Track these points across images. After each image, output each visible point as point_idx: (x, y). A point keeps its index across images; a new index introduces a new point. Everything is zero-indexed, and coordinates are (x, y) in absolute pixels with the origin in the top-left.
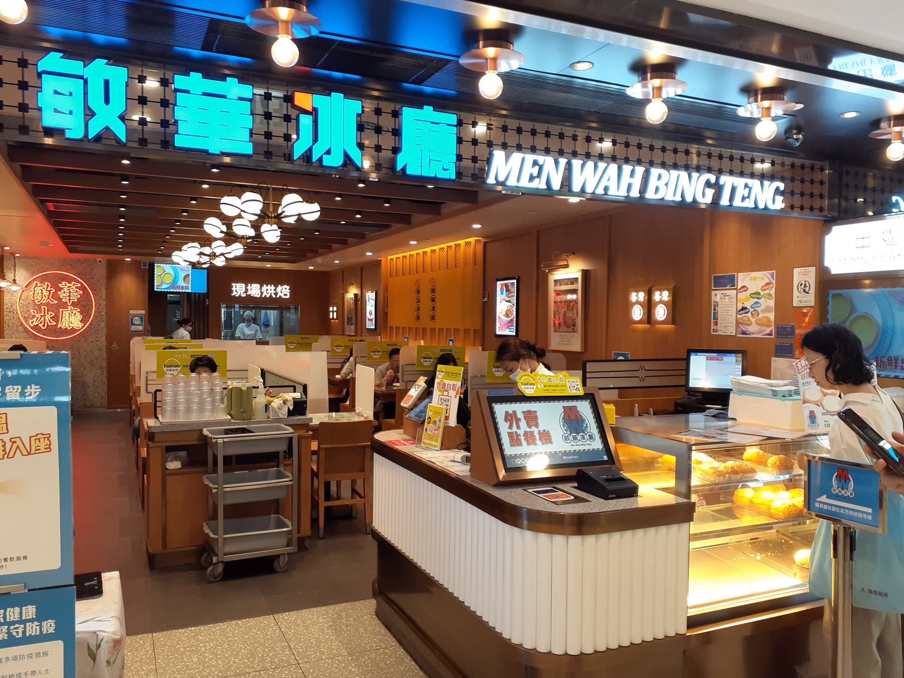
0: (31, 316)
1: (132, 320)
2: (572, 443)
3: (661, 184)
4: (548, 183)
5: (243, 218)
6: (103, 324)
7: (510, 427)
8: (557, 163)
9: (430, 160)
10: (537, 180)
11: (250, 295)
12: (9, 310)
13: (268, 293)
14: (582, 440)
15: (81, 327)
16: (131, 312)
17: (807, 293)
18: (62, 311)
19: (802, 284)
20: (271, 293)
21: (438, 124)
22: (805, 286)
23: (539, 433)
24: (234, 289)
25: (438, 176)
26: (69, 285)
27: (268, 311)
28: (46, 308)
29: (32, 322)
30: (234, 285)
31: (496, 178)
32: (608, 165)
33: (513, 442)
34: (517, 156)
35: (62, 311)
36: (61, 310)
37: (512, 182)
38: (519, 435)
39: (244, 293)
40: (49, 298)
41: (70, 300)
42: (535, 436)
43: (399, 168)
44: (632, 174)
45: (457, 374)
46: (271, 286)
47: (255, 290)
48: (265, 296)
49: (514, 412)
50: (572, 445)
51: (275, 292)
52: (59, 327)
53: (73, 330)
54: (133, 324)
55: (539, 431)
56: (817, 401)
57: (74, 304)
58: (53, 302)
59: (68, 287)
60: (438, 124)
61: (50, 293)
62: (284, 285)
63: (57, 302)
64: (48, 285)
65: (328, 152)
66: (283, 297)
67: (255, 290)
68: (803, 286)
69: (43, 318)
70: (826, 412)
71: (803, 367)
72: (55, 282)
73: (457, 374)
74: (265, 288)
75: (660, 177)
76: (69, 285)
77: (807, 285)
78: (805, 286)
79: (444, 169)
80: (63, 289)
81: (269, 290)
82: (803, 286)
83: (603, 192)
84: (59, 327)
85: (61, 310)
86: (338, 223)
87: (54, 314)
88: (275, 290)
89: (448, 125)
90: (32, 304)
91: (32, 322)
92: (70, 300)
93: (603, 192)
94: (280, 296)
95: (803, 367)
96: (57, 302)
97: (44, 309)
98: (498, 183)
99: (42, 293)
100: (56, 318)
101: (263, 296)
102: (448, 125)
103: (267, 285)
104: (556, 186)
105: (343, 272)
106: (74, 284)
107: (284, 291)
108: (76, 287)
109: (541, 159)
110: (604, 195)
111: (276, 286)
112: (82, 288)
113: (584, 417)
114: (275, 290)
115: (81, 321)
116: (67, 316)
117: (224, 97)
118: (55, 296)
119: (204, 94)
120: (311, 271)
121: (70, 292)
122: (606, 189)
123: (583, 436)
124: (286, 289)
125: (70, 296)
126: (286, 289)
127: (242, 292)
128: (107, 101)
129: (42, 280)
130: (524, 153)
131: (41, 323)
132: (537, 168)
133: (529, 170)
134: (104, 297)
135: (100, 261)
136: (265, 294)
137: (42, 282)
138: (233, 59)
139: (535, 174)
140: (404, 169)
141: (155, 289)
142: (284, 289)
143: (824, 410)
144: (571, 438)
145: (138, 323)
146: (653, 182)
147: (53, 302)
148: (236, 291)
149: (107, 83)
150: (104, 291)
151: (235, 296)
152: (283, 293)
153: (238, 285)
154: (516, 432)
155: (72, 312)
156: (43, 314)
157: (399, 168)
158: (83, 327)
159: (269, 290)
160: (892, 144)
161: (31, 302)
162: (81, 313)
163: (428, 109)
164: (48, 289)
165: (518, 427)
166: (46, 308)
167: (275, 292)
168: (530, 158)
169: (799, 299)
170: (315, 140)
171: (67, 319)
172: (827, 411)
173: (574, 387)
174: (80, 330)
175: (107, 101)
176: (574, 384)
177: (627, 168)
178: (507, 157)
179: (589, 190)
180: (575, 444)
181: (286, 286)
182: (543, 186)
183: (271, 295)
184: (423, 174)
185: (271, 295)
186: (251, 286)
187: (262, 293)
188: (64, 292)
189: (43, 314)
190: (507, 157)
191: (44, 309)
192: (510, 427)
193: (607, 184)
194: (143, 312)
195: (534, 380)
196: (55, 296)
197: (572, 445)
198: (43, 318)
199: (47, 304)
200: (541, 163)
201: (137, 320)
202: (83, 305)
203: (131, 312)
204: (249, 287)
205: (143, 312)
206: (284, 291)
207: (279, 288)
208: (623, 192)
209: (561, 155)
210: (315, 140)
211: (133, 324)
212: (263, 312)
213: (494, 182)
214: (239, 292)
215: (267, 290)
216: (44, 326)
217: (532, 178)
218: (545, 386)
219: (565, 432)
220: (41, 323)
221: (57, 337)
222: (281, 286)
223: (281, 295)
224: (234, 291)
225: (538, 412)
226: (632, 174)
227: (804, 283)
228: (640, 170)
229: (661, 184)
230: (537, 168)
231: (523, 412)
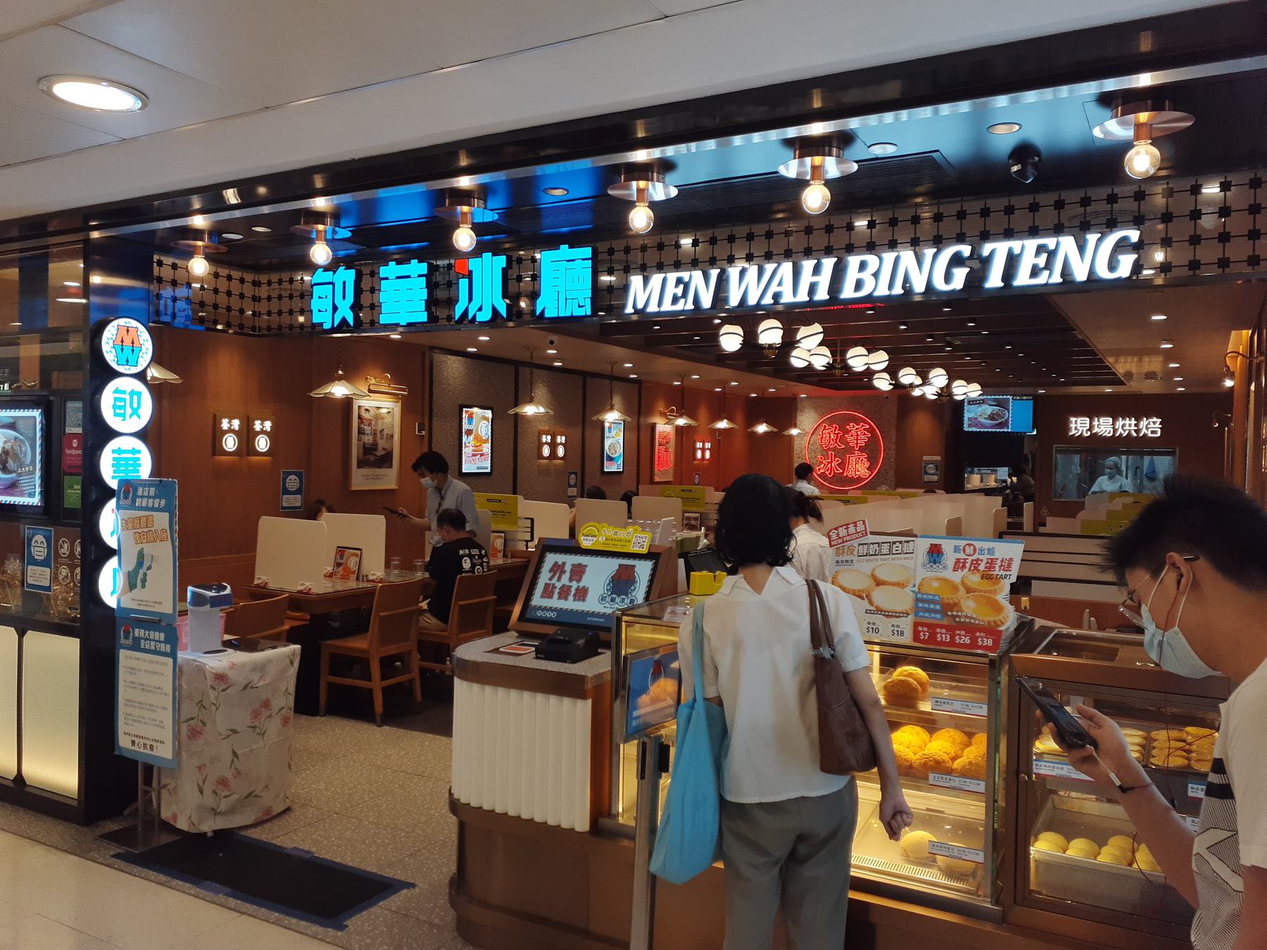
1: (925, 467)
2: (607, 605)
3: (867, 276)
4: (696, 301)
5: (818, 346)
6: (892, 473)
7: (551, 579)
8: (706, 277)
9: (566, 299)
10: (682, 301)
11: (1096, 433)
12: (798, 456)
13: (1124, 430)
14: (620, 604)
15: (868, 475)
16: (925, 458)
18: (849, 457)
20: (1130, 430)
21: (573, 260)
24: (1073, 425)
25: (574, 314)
26: (857, 427)
28: (833, 453)
29: (819, 470)
30: (1073, 419)
31: (634, 306)
32: (779, 264)
33: (545, 593)
34: (657, 279)
35: (849, 457)
36: (848, 456)
37: (653, 308)
38: (556, 588)
39: (1087, 430)
40: (836, 442)
41: (857, 444)
42: (571, 591)
43: (538, 312)
44: (817, 270)
45: (503, 512)
46: (1130, 420)
47: (1104, 426)
48: (1121, 434)
49: (564, 564)
51: (1136, 428)
52: (845, 475)
53: (860, 479)
54: (926, 473)
55: (579, 586)
56: (859, 591)
57: (861, 449)
58: (840, 446)
59: (857, 429)
60: (573, 260)
61: (837, 436)
62: (1152, 418)
63: (844, 447)
64: (836, 428)
65: (480, 309)
66: (1150, 435)
67: (1104, 426)
69: (830, 465)
70: (873, 608)
71: (840, 538)
72: (842, 424)
73: (503, 512)
74: (1120, 422)
75: (863, 266)
76: (857, 427)
79: (579, 306)
80: (850, 431)
81: (1126, 426)
83: (772, 302)
84: (845, 475)
85: (848, 456)
86: (980, 334)
87: (840, 461)
89: (583, 259)
90: (820, 449)
91: (819, 470)
92: (857, 444)
93: (772, 302)
94: (1145, 435)
95: (840, 538)
96: (844, 447)
97: (832, 454)
98: (637, 311)
99: (830, 437)
100: (842, 465)
101: (1117, 435)
102: (583, 259)
103: (1123, 419)
104: (706, 302)
106: (863, 426)
107: (1151, 427)
108: (864, 429)
109: (685, 275)
110: (773, 304)
111: (1138, 419)
112: (871, 430)
113: (637, 579)
114: (1136, 425)
115: (868, 469)
117: (408, 277)
118: (842, 439)
119: (398, 278)
120: (1181, 393)
121: (858, 435)
122: (776, 296)
123: (623, 599)
124: (1154, 423)
125: (857, 440)
126: (1154, 423)
127: (1085, 429)
128: (344, 298)
129: (831, 421)
130: (665, 273)
131: (827, 470)
132: (682, 286)
133: (671, 290)
134: (894, 439)
135: (887, 398)
136: (1120, 430)
137: (830, 425)
138: (392, 247)
139: (680, 294)
140: (543, 312)
141: (966, 428)
142: (1151, 423)
143: (872, 605)
144: (608, 599)
145: (933, 472)
146: (852, 275)
147: (840, 446)
148: (1076, 428)
149: (344, 283)
150: (894, 433)
151: (1074, 435)
152: (1150, 430)
153: (1079, 420)
155: (859, 459)
156: (830, 461)
157: (538, 312)
158: (870, 476)
159: (1126, 426)
161: (819, 446)
162: (869, 459)
163: (564, 247)
164: (836, 432)
166: (833, 453)
167: (1136, 428)
168: (672, 277)
170: (470, 299)
171: (854, 466)
172: (876, 607)
173: (639, 543)
174: (867, 479)
175: (344, 298)
176: (640, 540)
177: (808, 265)
178: (646, 281)
179: (752, 301)
180: (609, 606)
181: (1155, 419)
182: (690, 306)
183: (1129, 434)
184: (560, 315)
185: (1129, 434)
186: (1098, 421)
187: (1115, 431)
188: (852, 436)
189: (830, 461)
190: (646, 281)
191: (832, 454)
192: (551, 579)
193: (779, 289)
194: (939, 458)
195: (598, 531)
196: (842, 439)
197: (605, 607)
198: (830, 465)
199: (834, 449)
200: (686, 279)
201: (931, 469)
202: (870, 450)
203: (925, 458)
204: (1096, 423)
205: (939, 458)
206: (1151, 427)
207: (1144, 423)
208: (803, 296)
209: (677, 268)
210: (470, 299)
211: (926, 473)
212: (1147, 459)
213: (633, 311)
214: (1081, 429)
215: (1124, 426)
216: (830, 474)
217: (675, 300)
218: (606, 539)
219: (606, 592)
220: (827, 470)
221: (843, 486)
222: (1147, 419)
223: (1147, 432)
224: (1073, 429)
225: (557, 561)
226: (817, 270)
228: (829, 263)
229: (867, 276)
230: (682, 286)
231: (586, 566)
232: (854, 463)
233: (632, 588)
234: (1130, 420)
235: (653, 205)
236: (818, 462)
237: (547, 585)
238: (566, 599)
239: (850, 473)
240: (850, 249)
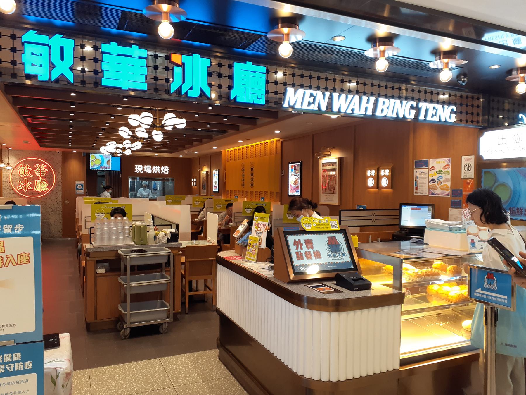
1: (77, 186)
2: (333, 258)
3: (385, 107)
4: (319, 106)
5: (141, 127)
6: (60, 189)
7: (297, 249)
8: (324, 95)
9: (250, 93)
10: (312, 105)
11: (145, 172)
12: (5, 181)
13: (156, 171)
14: (339, 256)
15: (47, 190)
16: (76, 182)
17: (470, 171)
18: (36, 181)
19: (466, 165)
20: (158, 171)
21: (255, 72)
22: (469, 166)
23: (314, 252)
24: (136, 168)
25: (255, 103)
26: (40, 166)
28: (27, 179)
29: (19, 188)
30: (136, 166)
31: (289, 104)
32: (354, 96)
33: (298, 257)
34: (301, 91)
35: (36, 181)
36: (35, 181)
37: (298, 106)
38: (302, 254)
39: (142, 171)
40: (28, 174)
41: (40, 175)
42: (311, 254)
43: (232, 98)
44: (368, 101)
46: (158, 167)
47: (148, 169)
48: (154, 172)
49: (299, 240)
51: (160, 170)
52: (34, 190)
53: (43, 192)
54: (77, 189)
55: (314, 251)
56: (475, 234)
57: (43, 177)
58: (31, 176)
59: (40, 167)
60: (255, 72)
61: (29, 171)
62: (165, 166)
63: (33, 176)
64: (28, 166)
65: (191, 89)
66: (165, 173)
67: (148, 169)
68: (467, 167)
69: (25, 186)
70: (480, 240)
71: (467, 214)
74: (154, 168)
75: (384, 103)
76: (40, 166)
77: (470, 166)
78: (469, 166)
79: (258, 99)
80: (36, 168)
81: (156, 169)
82: (467, 167)
83: (351, 112)
84: (34, 190)
85: (35, 181)
86: (197, 130)
87: (31, 183)
88: (160, 169)
89: (261, 73)
90: (18, 177)
91: (19, 188)
92: (40, 175)
94: (163, 173)
95: (467, 214)
96: (33, 176)
97: (26, 180)
98: (290, 107)
99: (24, 171)
100: (32, 185)
101: (153, 172)
102: (261, 73)
103: (155, 166)
104: (324, 108)
105: (199, 158)
106: (43, 166)
107: (165, 170)
108: (44, 167)
109: (315, 92)
110: (351, 113)
111: (161, 167)
112: (48, 168)
113: (340, 243)
114: (160, 169)
115: (47, 187)
117: (130, 56)
118: (32, 173)
119: (119, 55)
120: (181, 158)
121: (41, 170)
122: (353, 110)
123: (339, 254)
124: (166, 168)
126: (166, 168)
127: (141, 170)
128: (62, 59)
130: (305, 89)
131: (24, 188)
132: (312, 98)
133: (308, 99)
134: (61, 173)
135: (58, 152)
136: (154, 171)
137: (24, 165)
138: (135, 34)
139: (311, 101)
140: (235, 98)
141: (90, 169)
142: (165, 168)
143: (480, 239)
144: (332, 255)
145: (81, 188)
146: (380, 106)
147: (31, 176)
148: (137, 170)
149: (62, 48)
150: (60, 169)
152: (165, 171)
153: (139, 166)
154: (300, 252)
155: (42, 182)
156: (25, 183)
157: (232, 98)
158: (48, 191)
159: (156, 169)
161: (18, 176)
162: (47, 182)
163: (249, 63)
164: (28, 168)
166: (27, 179)
167: (160, 170)
168: (308, 92)
169: (465, 174)
170: (184, 81)
172: (481, 239)
173: (334, 225)
174: (46, 192)
175: (62, 59)
176: (334, 224)
177: (365, 98)
178: (295, 92)
179: (343, 110)
180: (335, 259)
181: (166, 167)
182: (316, 108)
183: (158, 172)
184: (246, 102)
185: (158, 172)
186: (146, 167)
187: (152, 171)
188: (37, 170)
189: (25, 183)
190: (295, 92)
191: (26, 180)
192: (297, 249)
193: (353, 107)
194: (83, 182)
195: (311, 221)
196: (32, 173)
197: (333, 259)
198: (25, 186)
199: (27, 177)
200: (315, 95)
201: (80, 187)
202: (48, 178)
203: (76, 182)
204: (145, 167)
205: (83, 182)
206: (165, 170)
207: (162, 168)
208: (362, 112)
209: (326, 91)
210: (184, 81)
211: (77, 189)
212: (153, 182)
213: (288, 106)
214: (139, 170)
215: (155, 169)
216: (25, 190)
217: (309, 104)
218: (317, 225)
219: (329, 252)
220: (24, 188)
221: (33, 196)
222: (164, 167)
223: (164, 172)
224: (136, 170)
225: (313, 240)
226: (368, 101)
227: (468, 165)
228: (372, 99)
230: (312, 98)
231: (304, 240)
232: (39, 184)
233: (340, 248)
234: (158, 167)
235: (388, 59)
236: (18, 184)
237: (297, 253)
238: (303, 259)
239: (37, 189)
240: (379, 95)
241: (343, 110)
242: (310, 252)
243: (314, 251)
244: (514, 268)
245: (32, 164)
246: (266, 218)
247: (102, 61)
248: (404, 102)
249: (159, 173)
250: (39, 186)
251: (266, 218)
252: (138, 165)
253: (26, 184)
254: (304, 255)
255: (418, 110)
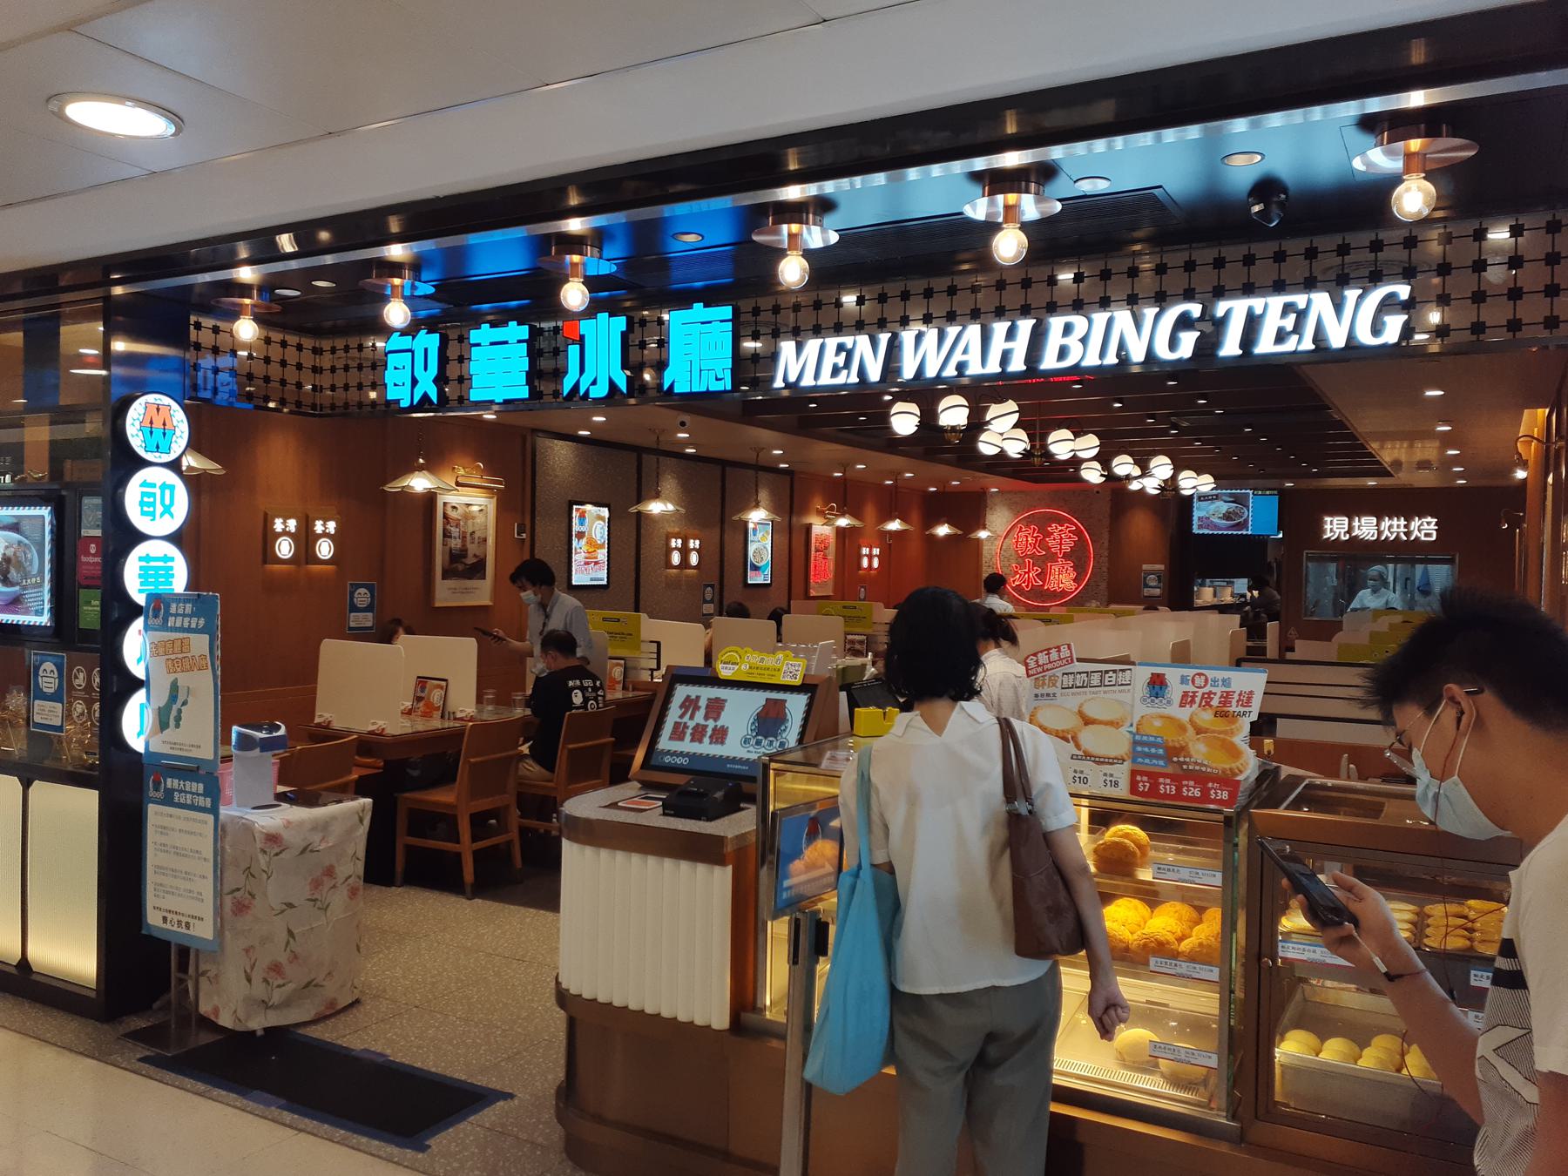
0: (1013, 572)
1: (1145, 578)
2: (751, 749)
3: (1073, 341)
4: (862, 372)
5: (1013, 428)
6: (1103, 585)
7: (682, 716)
8: (874, 343)
9: (701, 370)
10: (845, 372)
11: (1356, 537)
12: (987, 564)
13: (1391, 533)
14: (767, 747)
15: (1074, 588)
16: (1145, 567)
18: (1051, 566)
20: (1398, 533)
21: (710, 322)
23: (714, 730)
24: (1328, 527)
25: (711, 389)
26: (1060, 528)
27: (1430, 567)
28: (1031, 561)
29: (1014, 581)
30: (1328, 519)
31: (785, 379)
32: (964, 327)
33: (675, 734)
34: (812, 345)
35: (1051, 566)
36: (1049, 564)
37: (808, 381)
38: (687, 728)
39: (1345, 533)
40: (1035, 548)
41: (1061, 549)
42: (706, 732)
43: (666, 387)
44: (1011, 334)
46: (1398, 520)
47: (1366, 528)
48: (1387, 538)
49: (698, 698)
50: (748, 751)
51: (1406, 530)
52: (1046, 588)
53: (1064, 593)
54: (1146, 586)
55: (716, 726)
56: (1063, 731)
57: (1066, 556)
58: (1039, 552)
59: (1060, 531)
60: (710, 322)
61: (1036, 540)
62: (1425, 517)
63: (1044, 553)
64: (1034, 529)
65: (594, 383)
66: (1423, 538)
67: (1366, 528)
69: (1027, 576)
70: (1081, 753)
71: (1039, 666)
74: (1386, 523)
75: (1068, 329)
76: (1060, 528)
79: (717, 379)
80: (1052, 534)
81: (1393, 527)
83: (956, 373)
84: (1046, 588)
85: (1049, 564)
86: (1212, 413)
87: (1040, 570)
88: (1405, 526)
89: (722, 321)
90: (1014, 556)
91: (1014, 581)
92: (1061, 549)
94: (1417, 538)
95: (1039, 666)
96: (1044, 553)
97: (1029, 562)
98: (788, 386)
99: (1027, 541)
100: (1042, 576)
101: (1383, 538)
102: (722, 321)
103: (1390, 518)
104: (874, 374)
106: (1068, 527)
107: (1425, 528)
108: (1070, 531)
109: (848, 341)
110: (956, 377)
111: (1408, 519)
112: (1078, 532)
113: (789, 717)
114: (1405, 526)
115: (1074, 581)
116: (1057, 573)
117: (506, 343)
118: (1042, 544)
119: (492, 344)
120: (1462, 487)
121: (1061, 539)
122: (961, 367)
123: (771, 741)
124: (1428, 523)
126: (1428, 523)
127: (1343, 531)
128: (426, 369)
130: (824, 338)
131: (1024, 582)
132: (844, 354)
133: (831, 358)
134: (1106, 544)
135: (1098, 492)
136: (1386, 533)
137: (1027, 526)
138: (486, 306)
139: (841, 364)
140: (672, 386)
141: (1196, 530)
142: (1425, 524)
144: (753, 742)
145: (1155, 584)
146: (1054, 340)
147: (1039, 552)
148: (1331, 530)
149: (426, 350)
150: (1106, 536)
151: (1329, 538)
152: (1423, 532)
153: (1336, 520)
154: (685, 723)
155: (1063, 568)
156: (1027, 570)
157: (666, 387)
158: (1076, 589)
159: (1393, 527)
160: (1406, 183)
161: (1013, 552)
162: (1075, 568)
163: (698, 306)
164: (1035, 535)
165: (692, 717)
166: (1031, 561)
167: (1406, 530)
168: (832, 343)
170: (582, 371)
172: (1084, 752)
173: (791, 672)
174: (1073, 592)
175: (426, 369)
176: (793, 669)
177: (1000, 328)
178: (799, 347)
179: (931, 373)
180: (754, 750)
181: (1429, 519)
182: (854, 379)
183: (1398, 537)
184: (693, 390)
185: (1398, 537)
186: (1359, 521)
187: (1380, 533)
188: (1054, 539)
189: (1027, 570)
190: (799, 347)
191: (1029, 562)
192: (682, 716)
193: (964, 358)
194: (1162, 567)
195: (740, 658)
196: (1042, 544)
197: (748, 751)
198: (1027, 576)
199: (1033, 556)
200: (849, 346)
201: (1152, 580)
202: (1077, 557)
203: (1145, 567)
204: (1356, 523)
205: (1162, 567)
206: (1425, 528)
207: (1416, 523)
208: (993, 367)
209: (838, 332)
210: (582, 371)
211: (1146, 586)
212: (1419, 568)
213: (783, 385)
215: (1390, 527)
216: (1027, 586)
217: (836, 371)
218: (750, 668)
219: (750, 732)
220: (1024, 582)
221: (1043, 602)
222: (1420, 519)
223: (1419, 535)
224: (1328, 531)
225: (690, 694)
226: (1011, 334)
228: (1025, 326)
229: (1073, 341)
230: (844, 354)
231: (725, 701)
234: (1398, 520)
241: (931, 373)
242: (706, 726)
243: (716, 726)
244: (1305, 896)
245: (1042, 524)
246: (623, 634)
247: (470, 359)
248: (1150, 312)
249: (1405, 538)
250: (1057, 576)
251: (623, 634)
252: (1332, 514)
253: (1029, 571)
254: (689, 731)
255: (1213, 329)
